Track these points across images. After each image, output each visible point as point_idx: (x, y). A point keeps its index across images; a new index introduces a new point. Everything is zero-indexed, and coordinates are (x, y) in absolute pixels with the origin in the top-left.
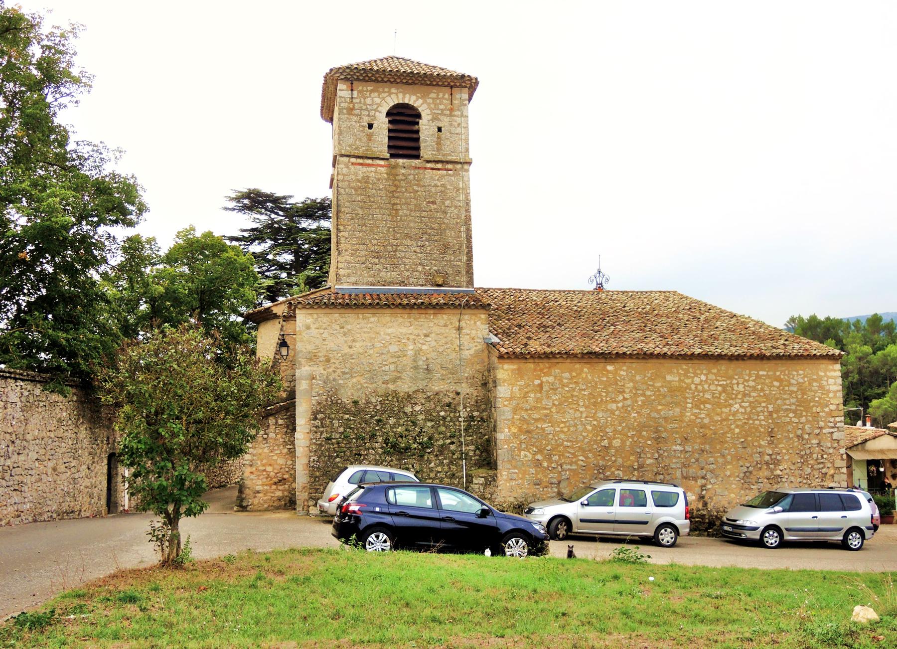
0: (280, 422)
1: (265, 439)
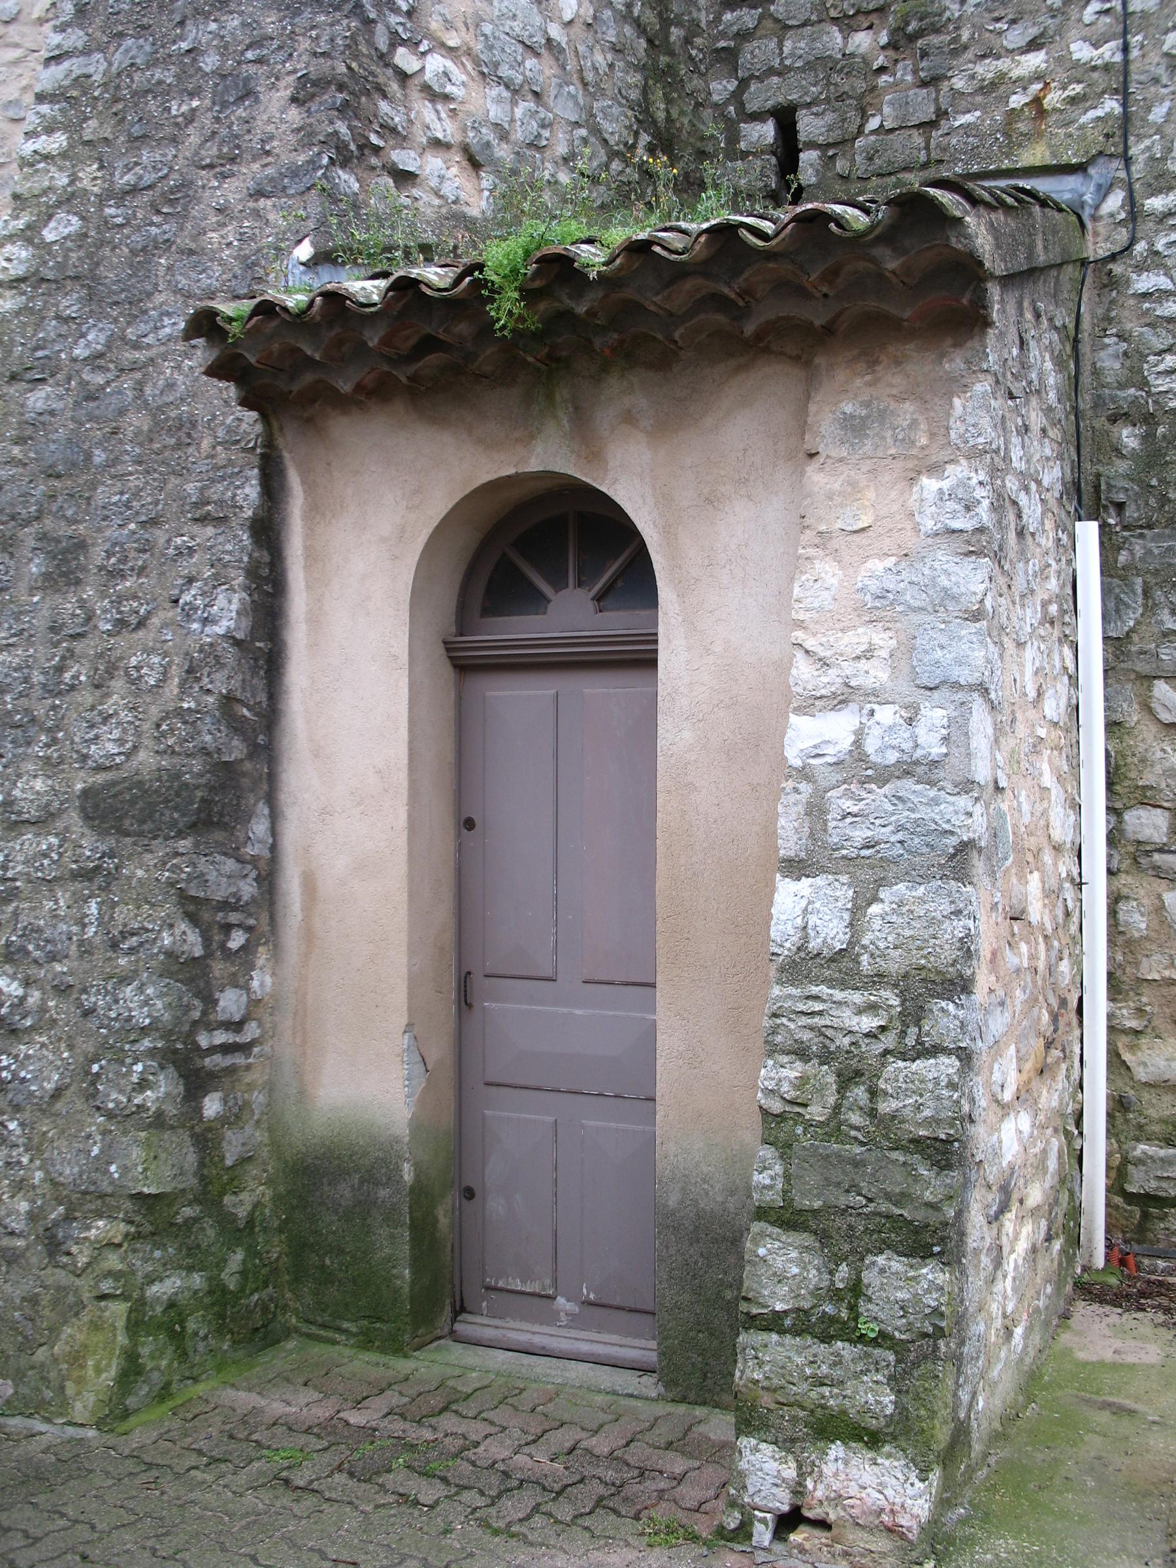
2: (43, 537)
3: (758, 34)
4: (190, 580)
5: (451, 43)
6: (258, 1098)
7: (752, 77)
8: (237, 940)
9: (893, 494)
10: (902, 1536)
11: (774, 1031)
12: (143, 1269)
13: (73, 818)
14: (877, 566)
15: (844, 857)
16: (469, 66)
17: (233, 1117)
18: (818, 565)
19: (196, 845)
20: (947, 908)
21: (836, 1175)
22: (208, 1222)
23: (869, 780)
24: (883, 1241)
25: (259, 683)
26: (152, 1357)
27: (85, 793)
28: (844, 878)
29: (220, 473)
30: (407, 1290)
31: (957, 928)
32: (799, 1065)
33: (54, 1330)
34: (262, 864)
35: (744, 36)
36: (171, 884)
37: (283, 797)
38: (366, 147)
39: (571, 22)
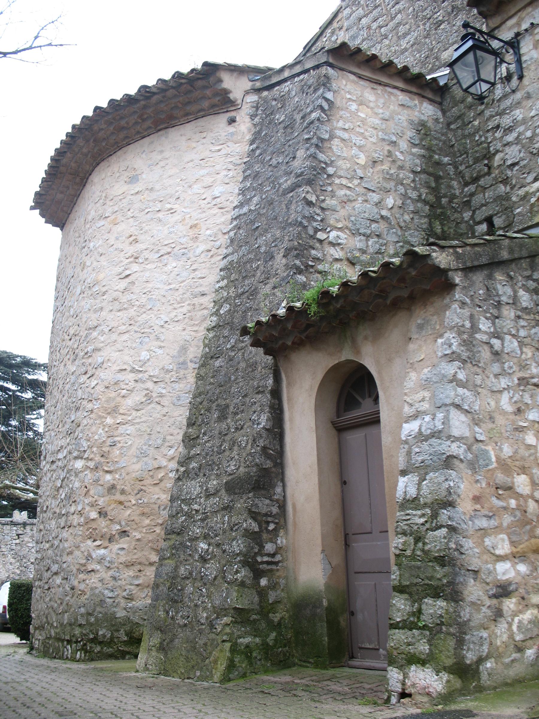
2: (218, 406)
3: (477, 192)
4: (255, 412)
5: (339, 226)
6: (282, 582)
7: (477, 209)
8: (271, 527)
9: (430, 346)
10: (431, 696)
11: (397, 528)
12: (237, 633)
13: (223, 491)
14: (426, 371)
15: (416, 467)
16: (347, 232)
17: (273, 586)
18: (410, 374)
19: (254, 495)
20: (444, 479)
21: (414, 573)
22: (263, 622)
23: (423, 440)
24: (427, 594)
25: (276, 442)
26: (239, 662)
27: (226, 482)
28: (416, 474)
29: (264, 378)
30: (326, 645)
31: (446, 485)
32: (404, 537)
33: (211, 653)
34: (280, 502)
35: (472, 195)
36: (246, 507)
37: (286, 479)
38: (307, 266)
39: (392, 208)
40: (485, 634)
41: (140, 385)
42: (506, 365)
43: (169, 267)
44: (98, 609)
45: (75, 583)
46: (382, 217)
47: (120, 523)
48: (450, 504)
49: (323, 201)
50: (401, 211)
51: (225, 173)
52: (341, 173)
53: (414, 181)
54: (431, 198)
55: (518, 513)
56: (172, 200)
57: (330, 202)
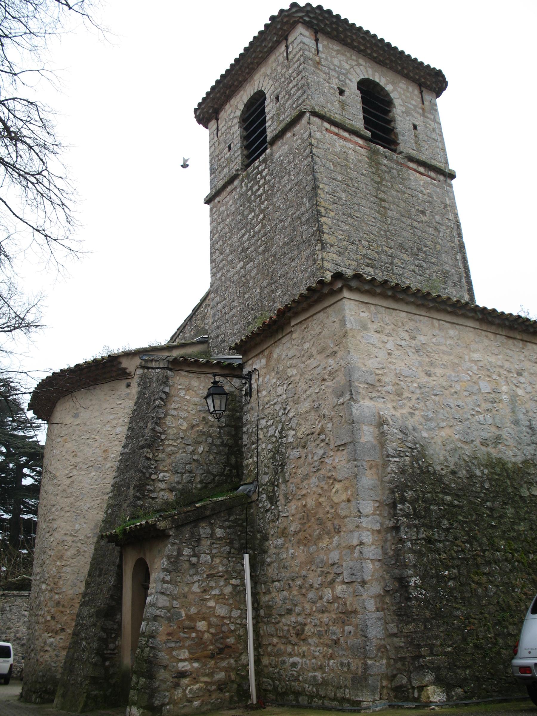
0: (219, 532)
1: (193, 565)
8: (113, 636)
13: (95, 616)
40: (167, 694)
41: (74, 544)
42: (199, 570)
43: (92, 475)
44: (48, 673)
45: (39, 657)
46: (194, 460)
47: (61, 624)
48: (154, 637)
49: (157, 456)
50: (208, 454)
51: (122, 419)
52: (170, 437)
53: (220, 433)
54: (231, 442)
55: (196, 640)
56: (95, 433)
57: (161, 456)
